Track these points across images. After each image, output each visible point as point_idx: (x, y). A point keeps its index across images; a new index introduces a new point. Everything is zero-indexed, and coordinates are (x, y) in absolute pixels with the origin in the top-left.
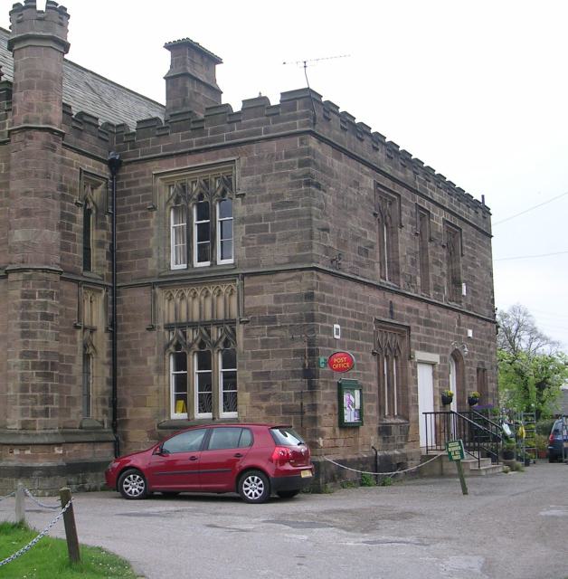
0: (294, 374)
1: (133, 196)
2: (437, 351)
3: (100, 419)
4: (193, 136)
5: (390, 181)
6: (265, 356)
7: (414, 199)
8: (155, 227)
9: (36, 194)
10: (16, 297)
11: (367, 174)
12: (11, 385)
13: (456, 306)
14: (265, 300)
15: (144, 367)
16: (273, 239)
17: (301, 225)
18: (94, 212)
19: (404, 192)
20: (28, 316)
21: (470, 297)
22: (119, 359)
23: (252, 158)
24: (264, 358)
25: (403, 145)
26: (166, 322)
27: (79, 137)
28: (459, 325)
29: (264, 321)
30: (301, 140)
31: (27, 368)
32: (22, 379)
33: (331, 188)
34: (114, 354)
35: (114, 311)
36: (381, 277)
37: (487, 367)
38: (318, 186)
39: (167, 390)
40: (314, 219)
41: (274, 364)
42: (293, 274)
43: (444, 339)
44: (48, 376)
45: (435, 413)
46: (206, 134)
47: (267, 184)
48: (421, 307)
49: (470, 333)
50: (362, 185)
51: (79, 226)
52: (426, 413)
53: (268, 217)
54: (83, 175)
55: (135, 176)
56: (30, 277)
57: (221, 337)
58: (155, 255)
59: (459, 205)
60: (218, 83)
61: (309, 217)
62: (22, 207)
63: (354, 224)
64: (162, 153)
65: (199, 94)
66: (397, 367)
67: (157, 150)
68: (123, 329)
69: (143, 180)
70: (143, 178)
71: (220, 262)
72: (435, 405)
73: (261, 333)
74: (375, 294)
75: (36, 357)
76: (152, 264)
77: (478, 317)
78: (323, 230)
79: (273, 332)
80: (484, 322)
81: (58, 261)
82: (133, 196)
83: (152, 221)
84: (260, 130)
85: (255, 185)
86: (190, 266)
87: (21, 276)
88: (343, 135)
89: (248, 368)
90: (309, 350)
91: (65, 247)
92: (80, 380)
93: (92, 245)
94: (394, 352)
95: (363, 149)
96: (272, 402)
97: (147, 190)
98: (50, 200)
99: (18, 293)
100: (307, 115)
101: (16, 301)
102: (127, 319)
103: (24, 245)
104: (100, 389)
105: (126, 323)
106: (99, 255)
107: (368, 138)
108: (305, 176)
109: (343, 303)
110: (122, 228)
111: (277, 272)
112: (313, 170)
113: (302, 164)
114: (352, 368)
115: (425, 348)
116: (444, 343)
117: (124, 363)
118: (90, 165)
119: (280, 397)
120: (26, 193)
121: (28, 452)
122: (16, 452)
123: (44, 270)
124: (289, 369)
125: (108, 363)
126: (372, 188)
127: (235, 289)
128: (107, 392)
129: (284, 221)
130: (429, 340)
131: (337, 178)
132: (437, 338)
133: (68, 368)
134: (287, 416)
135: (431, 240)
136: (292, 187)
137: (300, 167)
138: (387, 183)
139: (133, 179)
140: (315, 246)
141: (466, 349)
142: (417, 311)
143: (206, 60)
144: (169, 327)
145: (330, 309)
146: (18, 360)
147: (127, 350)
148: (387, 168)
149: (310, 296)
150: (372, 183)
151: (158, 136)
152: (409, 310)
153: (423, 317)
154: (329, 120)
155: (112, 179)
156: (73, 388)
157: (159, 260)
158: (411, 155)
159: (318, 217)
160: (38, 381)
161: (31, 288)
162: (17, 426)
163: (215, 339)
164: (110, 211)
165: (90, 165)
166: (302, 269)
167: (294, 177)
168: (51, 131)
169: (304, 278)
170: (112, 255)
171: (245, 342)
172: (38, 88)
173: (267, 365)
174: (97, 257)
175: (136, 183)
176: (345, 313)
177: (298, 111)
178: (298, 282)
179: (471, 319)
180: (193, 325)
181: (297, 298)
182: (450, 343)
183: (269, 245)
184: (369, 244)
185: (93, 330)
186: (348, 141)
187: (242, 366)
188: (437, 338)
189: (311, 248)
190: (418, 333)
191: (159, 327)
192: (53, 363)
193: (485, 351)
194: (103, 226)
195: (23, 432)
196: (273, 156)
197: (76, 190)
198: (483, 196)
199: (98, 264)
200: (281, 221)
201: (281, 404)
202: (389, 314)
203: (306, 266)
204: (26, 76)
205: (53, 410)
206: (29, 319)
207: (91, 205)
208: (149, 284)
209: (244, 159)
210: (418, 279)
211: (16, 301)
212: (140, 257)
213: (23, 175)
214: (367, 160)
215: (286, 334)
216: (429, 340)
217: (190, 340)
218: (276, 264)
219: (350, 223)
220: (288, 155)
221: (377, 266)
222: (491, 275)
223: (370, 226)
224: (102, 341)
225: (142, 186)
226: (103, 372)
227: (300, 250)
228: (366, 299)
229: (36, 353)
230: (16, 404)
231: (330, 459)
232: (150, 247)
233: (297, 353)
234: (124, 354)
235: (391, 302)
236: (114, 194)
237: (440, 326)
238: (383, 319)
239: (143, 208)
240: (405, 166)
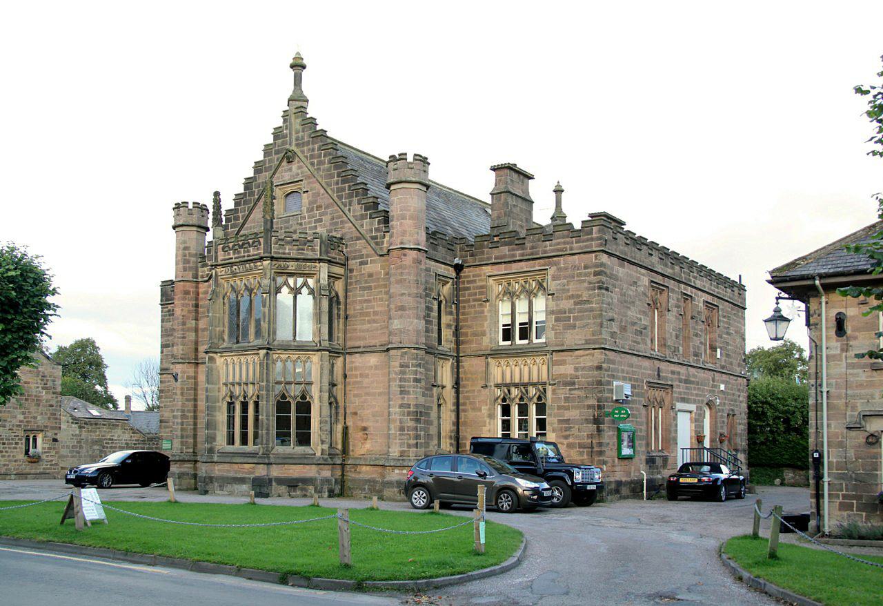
1: (472, 291)
2: (694, 401)
3: (448, 450)
4: (517, 250)
5: (661, 277)
6: (567, 408)
7: (679, 288)
8: (488, 315)
9: (409, 295)
10: (396, 367)
11: (643, 275)
12: (392, 426)
14: (567, 370)
15: (479, 413)
16: (574, 327)
17: (595, 317)
18: (444, 302)
19: (671, 284)
20: (405, 380)
21: (724, 358)
22: (461, 407)
23: (561, 268)
24: (566, 410)
25: (672, 248)
26: (496, 382)
27: (435, 249)
28: (713, 380)
29: (566, 384)
30: (596, 256)
31: (404, 415)
32: (401, 423)
33: (616, 289)
34: (457, 404)
35: (458, 373)
36: (652, 350)
37: (736, 412)
38: (607, 289)
39: (496, 430)
40: (604, 314)
41: (573, 414)
43: (700, 393)
44: (418, 421)
46: (527, 249)
47: (570, 287)
48: (682, 370)
49: (722, 387)
50: (639, 283)
51: (435, 314)
52: (683, 449)
53: (570, 311)
54: (437, 277)
55: (473, 277)
56: (406, 353)
57: (536, 394)
58: (488, 335)
59: (717, 288)
60: (530, 195)
61: (600, 312)
62: (400, 304)
63: (632, 313)
64: (493, 261)
65: (517, 206)
66: (662, 415)
67: (489, 258)
68: (464, 386)
69: (480, 280)
70: (480, 278)
71: (535, 341)
72: (691, 443)
73: (564, 392)
74: (646, 363)
75: (410, 408)
77: (731, 374)
78: (610, 320)
79: (573, 392)
80: (736, 378)
81: (424, 341)
82: (472, 291)
83: (486, 310)
84: (566, 248)
85: (561, 287)
86: (513, 343)
87: (399, 352)
88: (626, 249)
89: (555, 417)
90: (598, 405)
91: (427, 331)
92: (436, 422)
95: (641, 256)
96: (571, 440)
97: (482, 287)
98: (419, 299)
99: (397, 364)
100: (600, 238)
101: (395, 369)
102: (467, 379)
103: (401, 331)
104: (448, 429)
105: (467, 382)
106: (447, 334)
107: (645, 247)
108: (598, 282)
109: (623, 371)
110: (463, 314)
111: (577, 350)
112: (604, 278)
113: (596, 274)
114: (628, 417)
115: (683, 400)
116: (701, 396)
117: (464, 411)
119: (577, 437)
120: (403, 294)
121: (405, 471)
122: (397, 471)
123: (415, 348)
124: (584, 418)
125: (454, 411)
126: (647, 284)
127: (546, 361)
128: (453, 430)
129: (582, 314)
130: (688, 394)
131: (621, 281)
133: (428, 415)
134: (581, 450)
135: (692, 318)
136: (588, 290)
137: (594, 276)
138: (659, 279)
139: (472, 279)
140: (604, 332)
141: (718, 400)
142: (679, 373)
143: (522, 177)
144: (498, 386)
146: (398, 410)
147: (467, 401)
148: (659, 268)
149: (599, 368)
150: (647, 282)
151: (490, 248)
152: (673, 372)
153: (683, 378)
154: (616, 239)
155: (456, 278)
156: (431, 427)
157: (491, 338)
159: (606, 312)
160: (412, 424)
161: (406, 361)
162: (397, 454)
163: (531, 396)
164: (455, 302)
166: (594, 349)
167: (590, 283)
169: (596, 354)
170: (457, 333)
171: (552, 398)
172: (409, 219)
173: (568, 415)
174: (446, 335)
175: (474, 281)
177: (595, 235)
178: (591, 358)
179: (724, 376)
180: (516, 385)
181: (591, 368)
182: (705, 395)
183: (571, 331)
184: (643, 327)
185: (443, 387)
186: (631, 253)
187: (550, 415)
189: (601, 334)
190: (680, 389)
191: (491, 386)
192: (421, 412)
193: (735, 401)
194: (451, 313)
195: (401, 458)
196: (575, 267)
197: (433, 289)
198: (740, 276)
199: (446, 341)
200: (580, 314)
201: (577, 441)
202: (656, 376)
203: (597, 346)
204: (401, 210)
205: (421, 443)
206: (406, 382)
207: (442, 297)
208: (483, 355)
209: (554, 268)
210: (681, 348)
211: (395, 369)
212: (476, 335)
213: (400, 282)
214: (644, 265)
215: (581, 393)
216: (688, 394)
217: (512, 396)
218: (576, 344)
219: (629, 313)
220: (586, 267)
221: (649, 342)
222: (744, 340)
223: (644, 313)
224: (449, 394)
225: (479, 284)
226: (451, 417)
227: (593, 335)
228: (640, 367)
229: (410, 405)
230: (396, 439)
232: (485, 329)
233: (589, 407)
234: (464, 404)
235: (659, 368)
236: (457, 290)
238: (652, 381)
239: (479, 300)
240: (673, 264)
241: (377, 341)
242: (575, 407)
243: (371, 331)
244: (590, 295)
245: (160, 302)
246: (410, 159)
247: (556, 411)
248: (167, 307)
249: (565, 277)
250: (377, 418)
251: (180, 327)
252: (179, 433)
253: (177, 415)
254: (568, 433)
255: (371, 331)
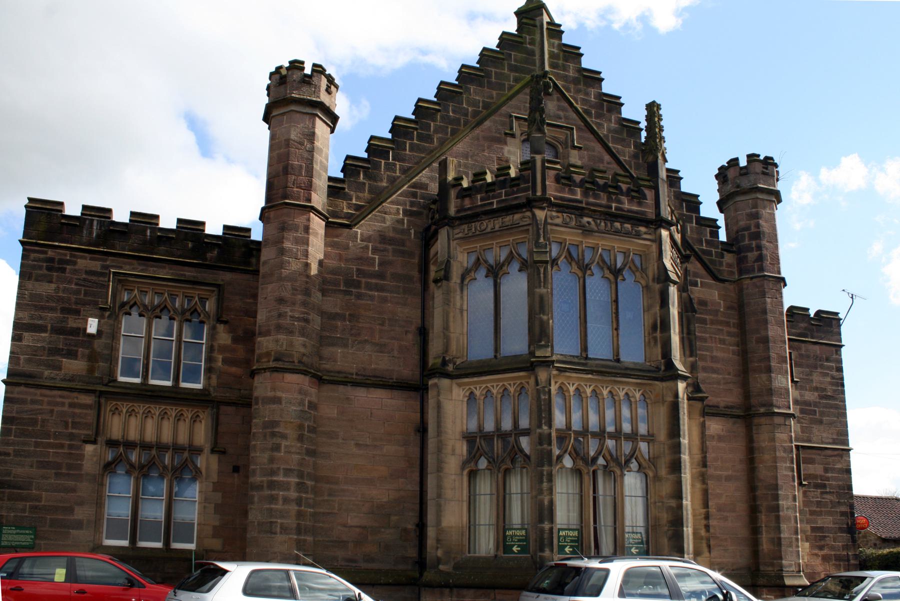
0: (841, 530)
6: (820, 514)
42: (836, 453)
45: (568, 493)
53: (816, 404)
79: (825, 496)
89: (807, 523)
119: (832, 548)
124: (837, 526)
132: (719, 366)
158: (759, 156)
173: (821, 522)
188: (719, 366)
241: (719, 399)
242: (830, 513)
243: (710, 383)
244: (835, 391)
245: (21, 238)
246: (743, 163)
247: (808, 516)
248: (46, 253)
249: (808, 366)
250: (725, 514)
251: (299, 297)
252: (291, 522)
253: (288, 483)
254: (823, 543)
255: (710, 383)
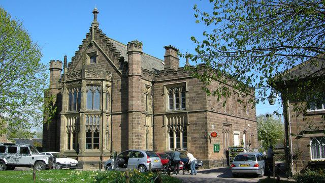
13: (245, 118)
16: (196, 103)
41: (197, 135)
74: (222, 116)
76: (164, 109)
93: (148, 104)
94: (228, 131)
96: (196, 145)
102: (157, 123)
115: (236, 130)
118: (147, 83)
145: (211, 121)
152: (232, 120)
165: (147, 83)
168: (139, 75)
170: (153, 106)
176: (215, 122)
181: (203, 118)
190: (234, 126)
194: (151, 99)
224: (151, 129)
231: (212, 160)
233: (203, 133)
234: (156, 133)
237: (240, 124)
